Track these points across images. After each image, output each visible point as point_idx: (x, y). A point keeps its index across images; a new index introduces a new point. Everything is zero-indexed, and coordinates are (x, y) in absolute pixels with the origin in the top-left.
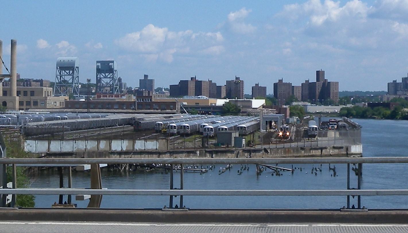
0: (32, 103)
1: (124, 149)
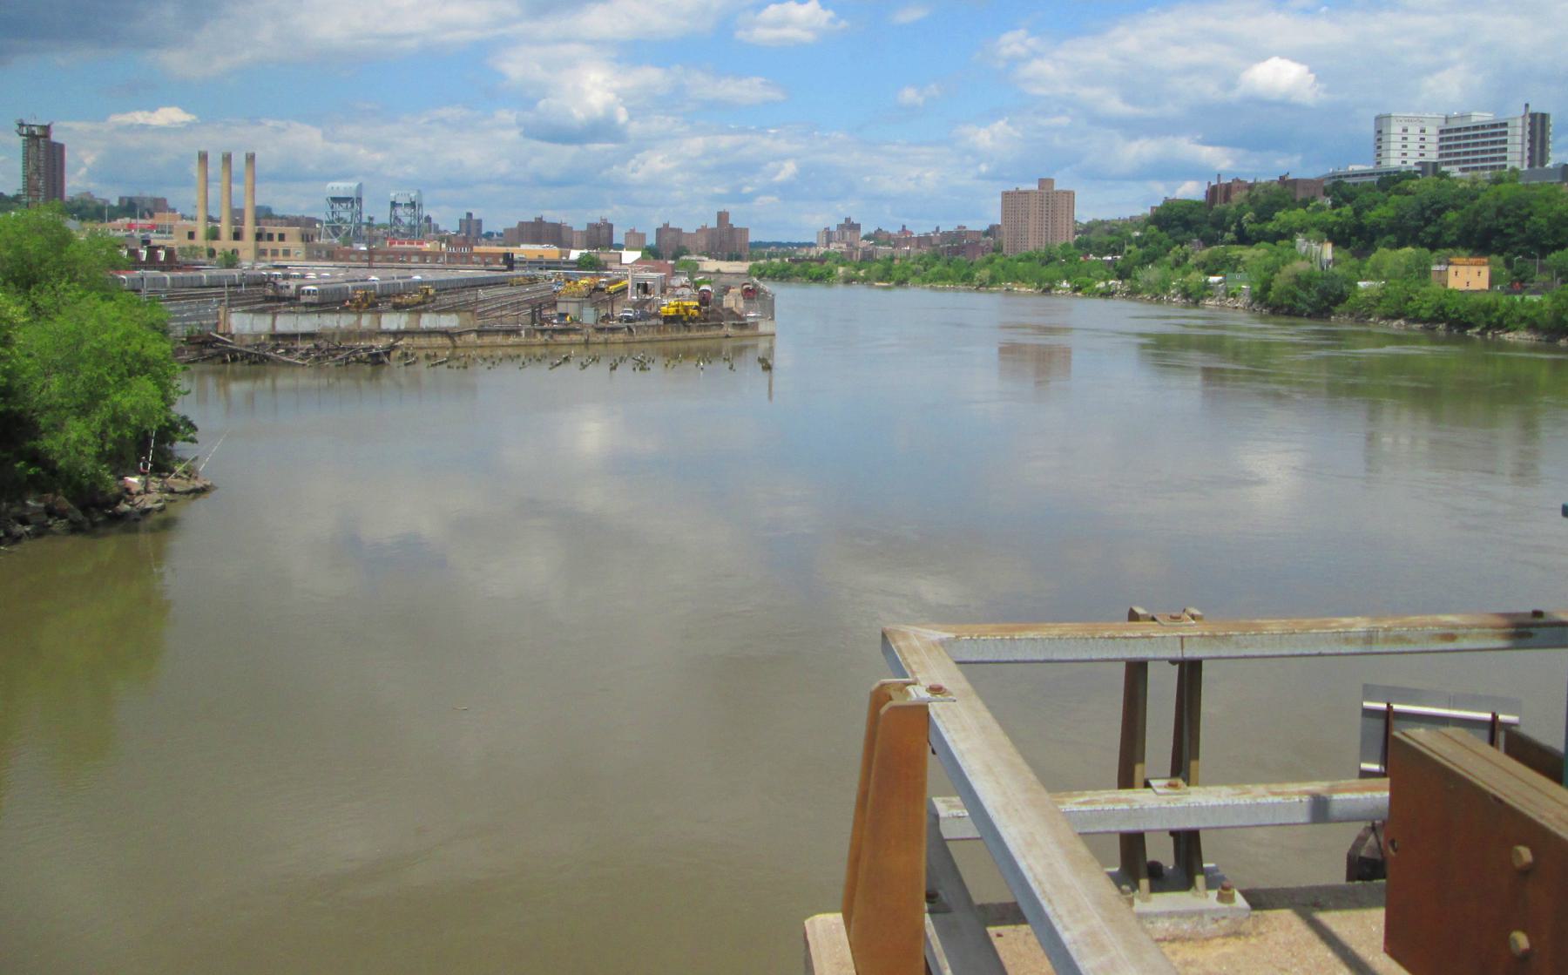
0: (281, 253)
1: (402, 327)
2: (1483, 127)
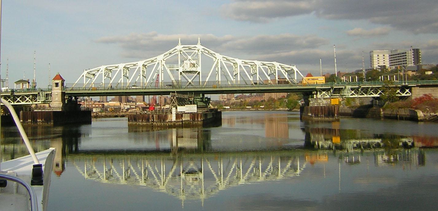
2: (400, 54)
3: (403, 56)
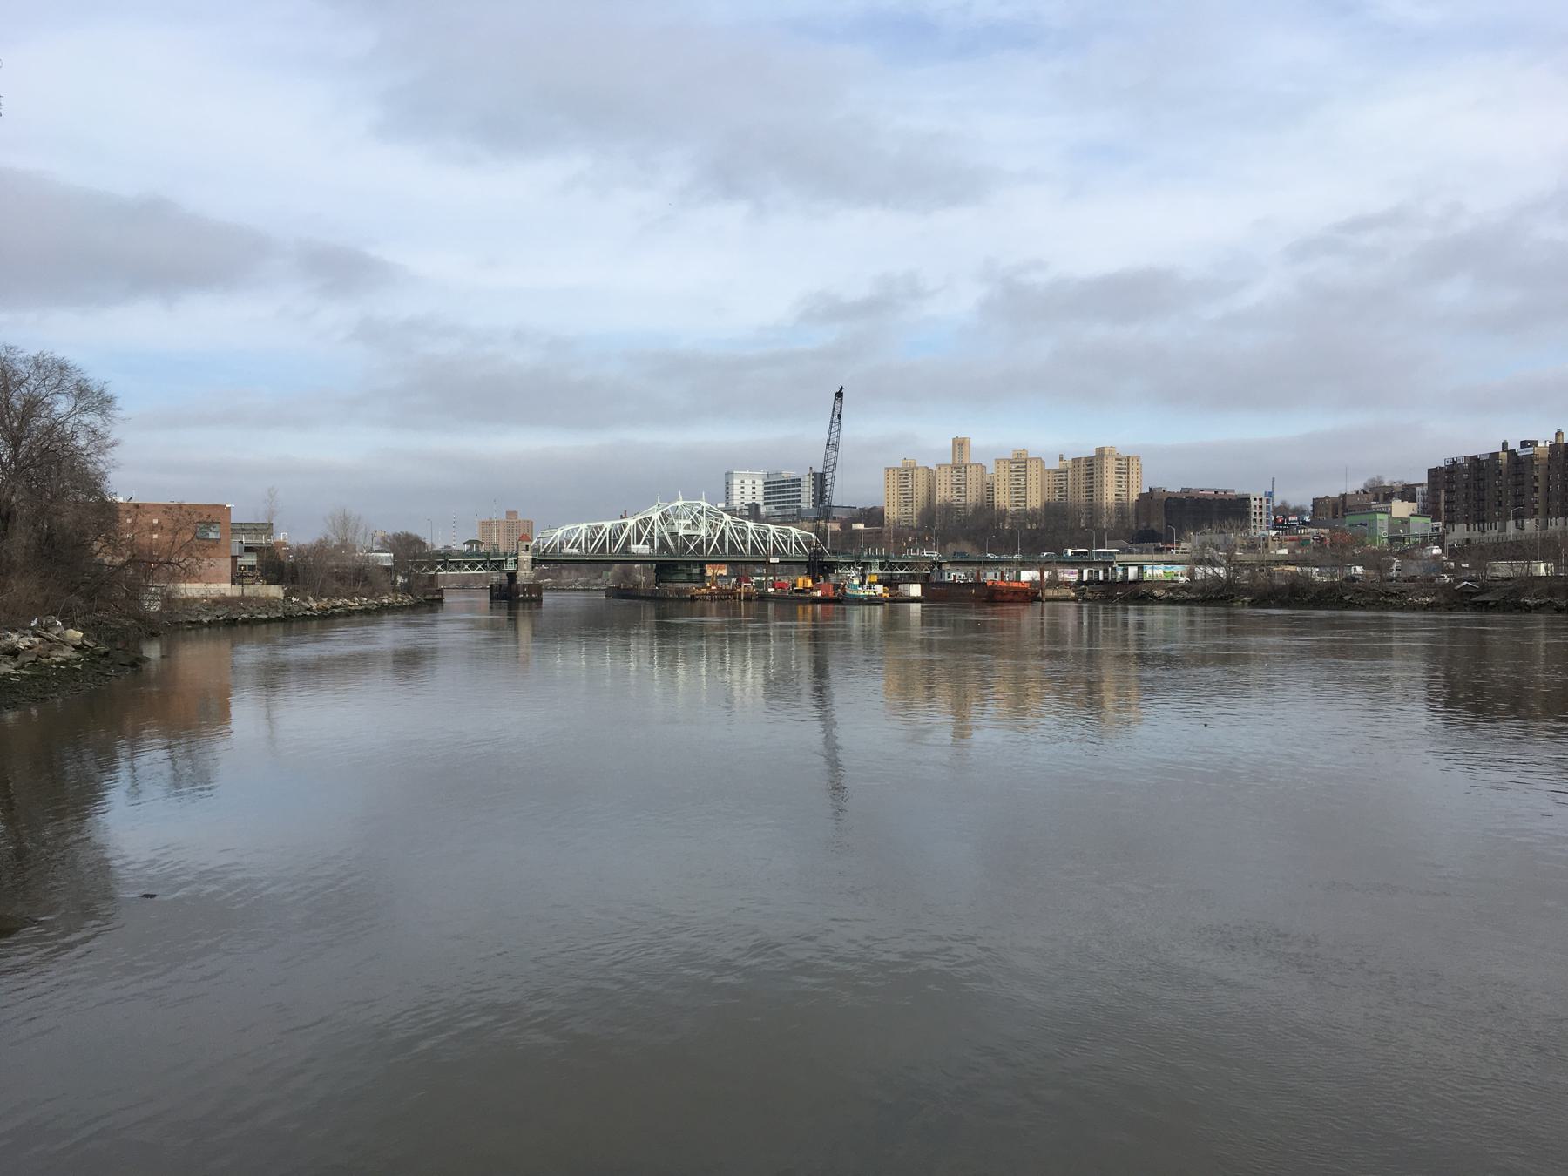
2: (788, 481)
3: (793, 486)
